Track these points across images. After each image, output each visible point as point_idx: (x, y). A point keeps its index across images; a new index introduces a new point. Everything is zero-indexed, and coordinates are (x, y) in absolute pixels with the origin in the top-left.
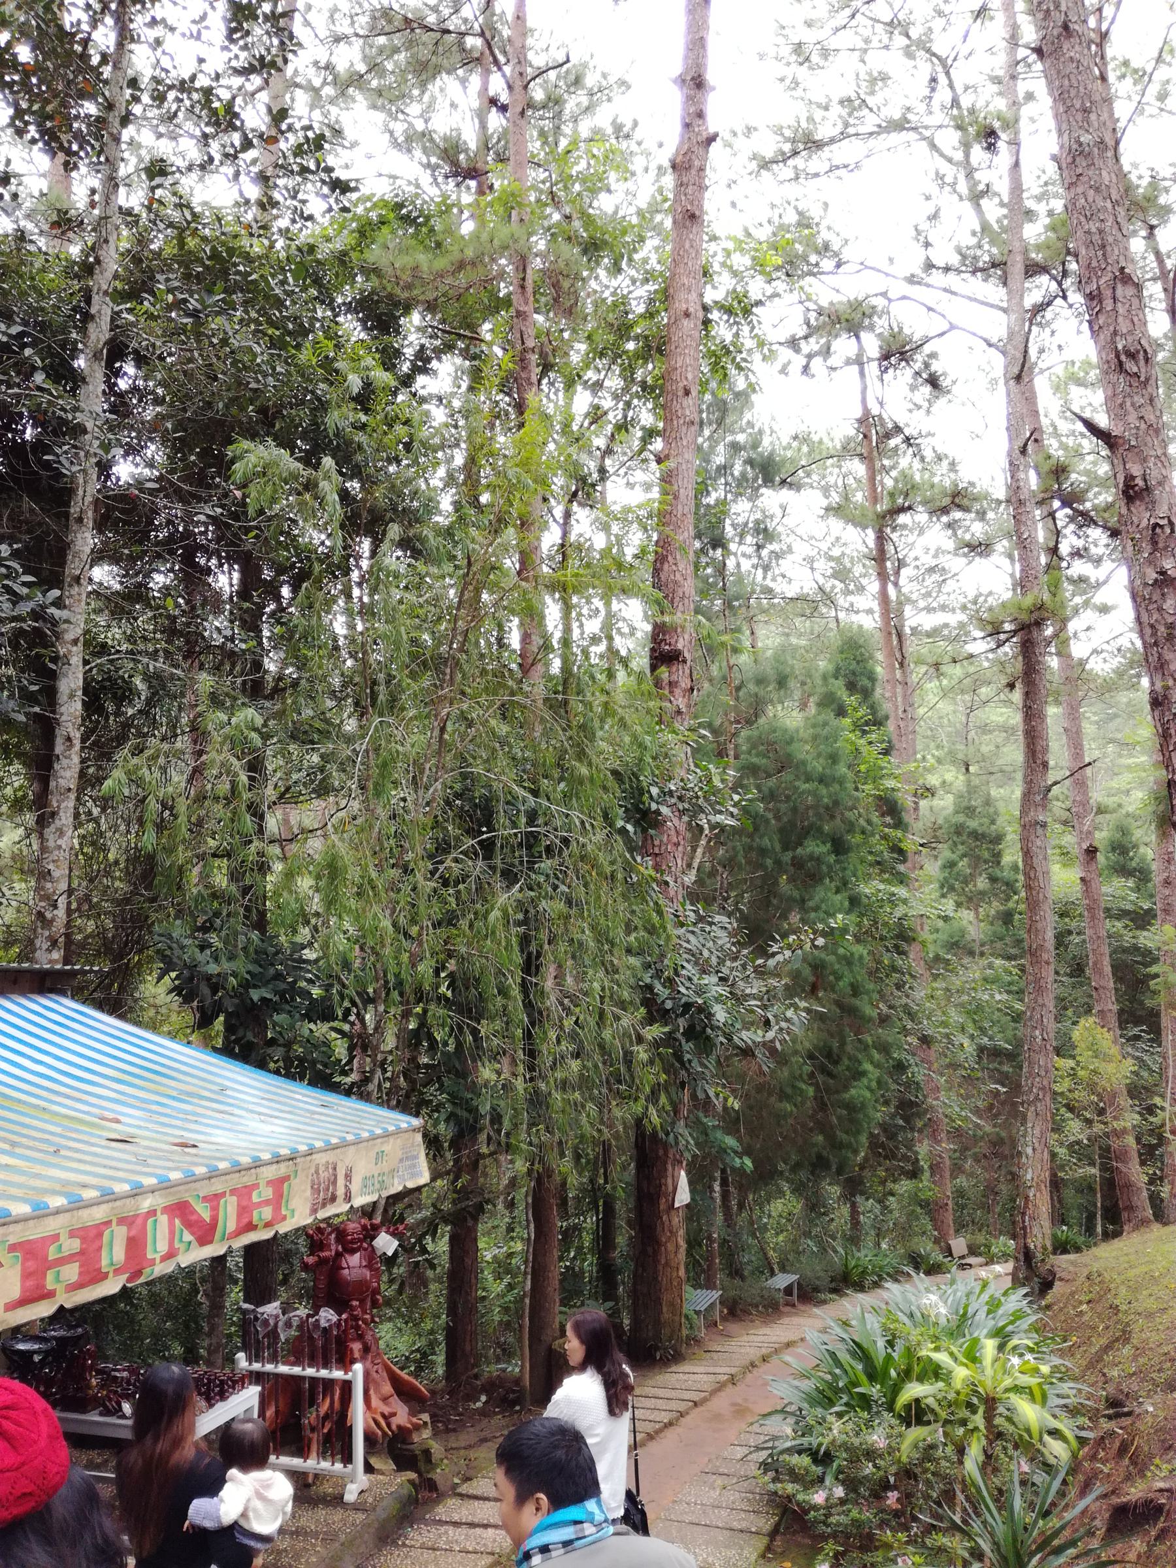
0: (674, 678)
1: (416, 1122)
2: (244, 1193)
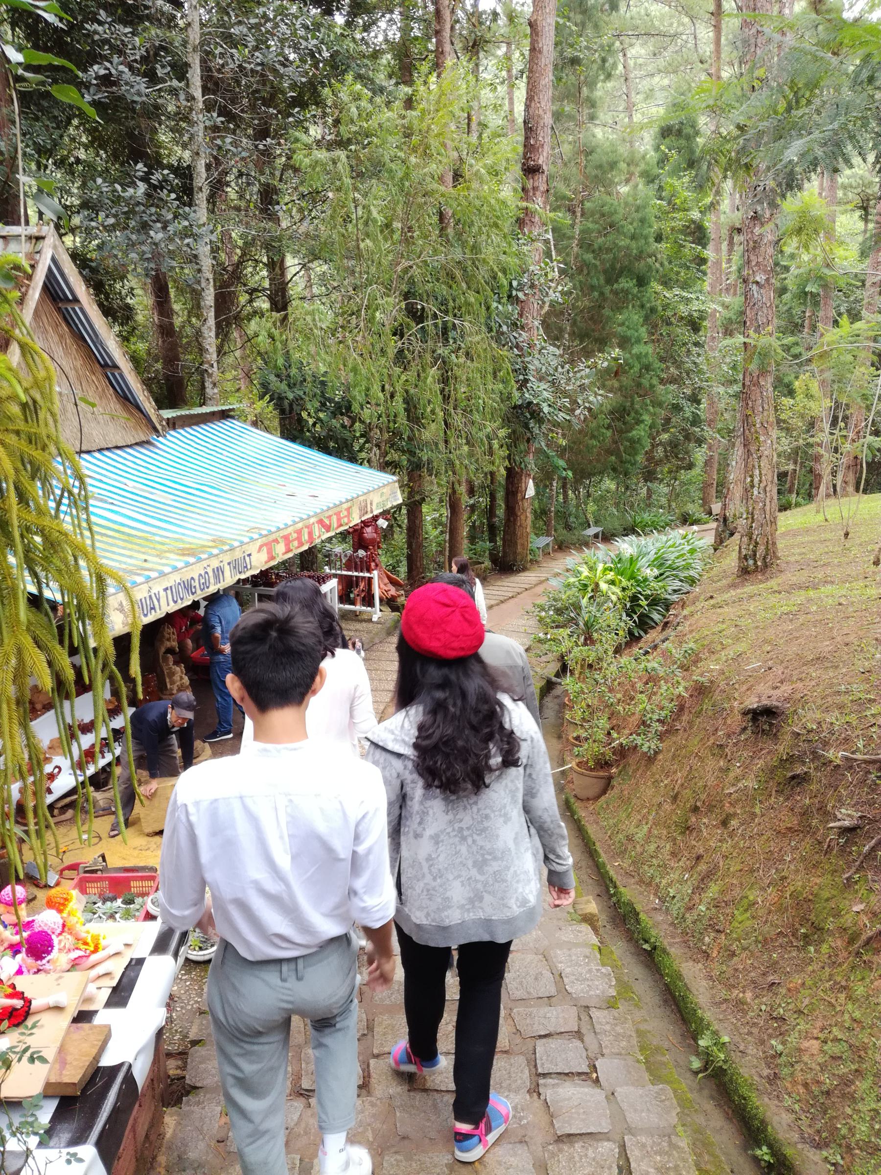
0: (536, 184)
1: (395, 478)
2: (338, 514)
